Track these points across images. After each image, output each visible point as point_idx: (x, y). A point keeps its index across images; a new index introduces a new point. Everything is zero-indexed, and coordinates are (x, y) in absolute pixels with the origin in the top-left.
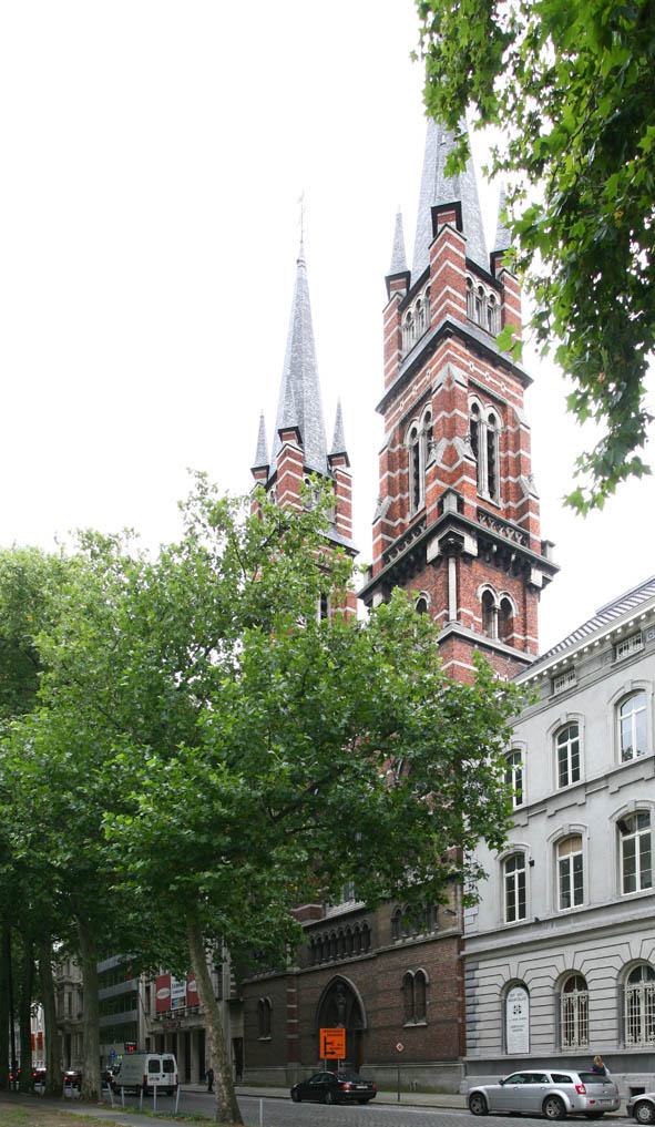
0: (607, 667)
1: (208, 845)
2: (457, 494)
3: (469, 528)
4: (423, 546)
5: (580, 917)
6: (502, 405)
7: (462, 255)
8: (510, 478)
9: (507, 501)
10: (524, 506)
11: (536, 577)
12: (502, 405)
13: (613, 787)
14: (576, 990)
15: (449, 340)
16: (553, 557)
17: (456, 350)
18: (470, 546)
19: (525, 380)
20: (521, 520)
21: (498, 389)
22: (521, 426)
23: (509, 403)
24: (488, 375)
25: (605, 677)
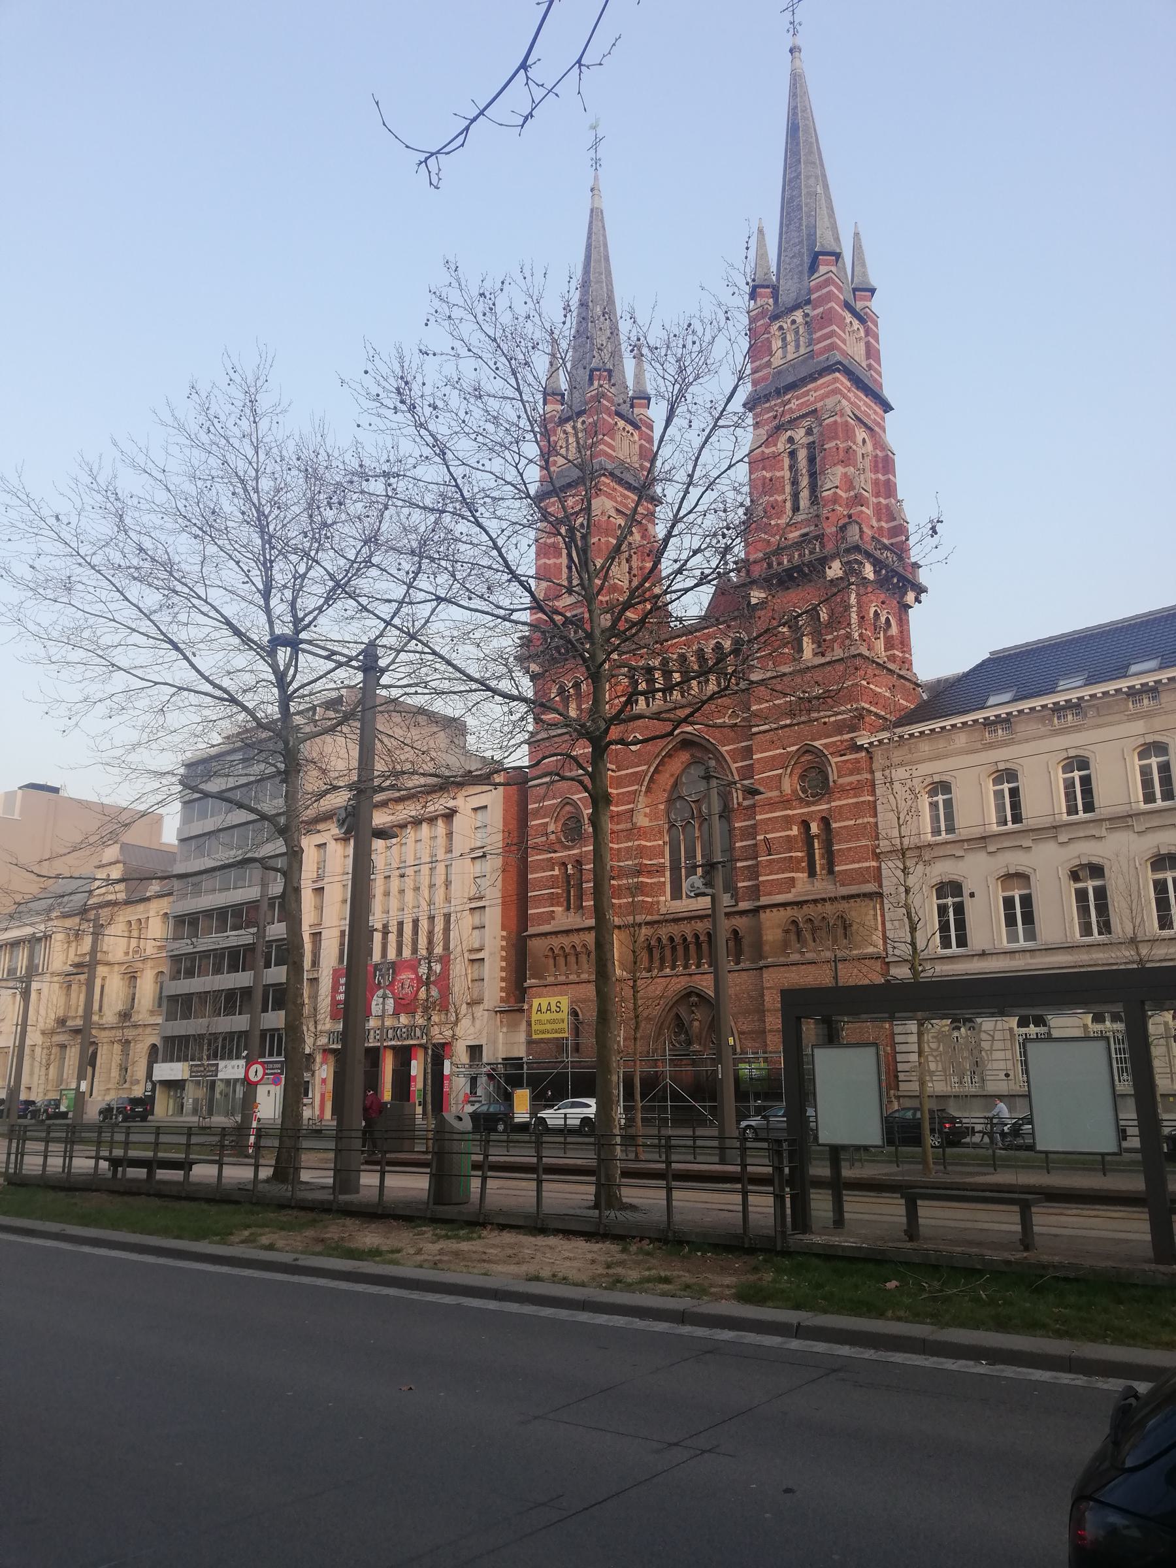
0: (1043, 730)
1: (581, 847)
2: (857, 523)
3: (868, 555)
4: (824, 561)
5: (956, 959)
6: (870, 429)
7: (842, 297)
8: (882, 500)
9: (879, 520)
10: (900, 530)
11: (910, 597)
12: (870, 429)
13: (1063, 838)
14: (1032, 1026)
15: (837, 374)
16: (923, 577)
17: (842, 384)
18: (869, 571)
19: (887, 407)
20: (893, 541)
21: (868, 416)
22: (890, 453)
23: (876, 429)
24: (864, 403)
25: (1041, 737)
